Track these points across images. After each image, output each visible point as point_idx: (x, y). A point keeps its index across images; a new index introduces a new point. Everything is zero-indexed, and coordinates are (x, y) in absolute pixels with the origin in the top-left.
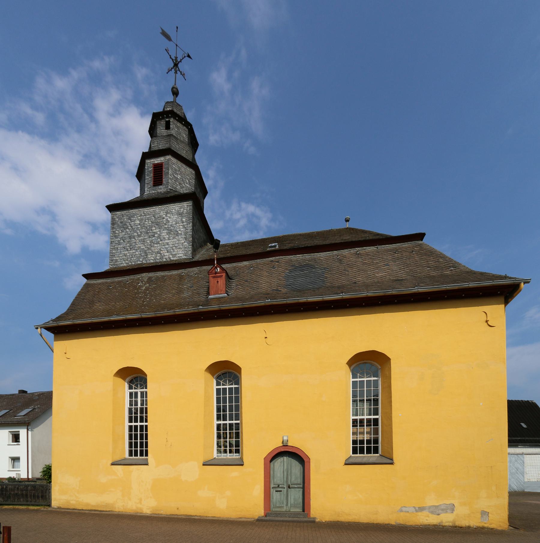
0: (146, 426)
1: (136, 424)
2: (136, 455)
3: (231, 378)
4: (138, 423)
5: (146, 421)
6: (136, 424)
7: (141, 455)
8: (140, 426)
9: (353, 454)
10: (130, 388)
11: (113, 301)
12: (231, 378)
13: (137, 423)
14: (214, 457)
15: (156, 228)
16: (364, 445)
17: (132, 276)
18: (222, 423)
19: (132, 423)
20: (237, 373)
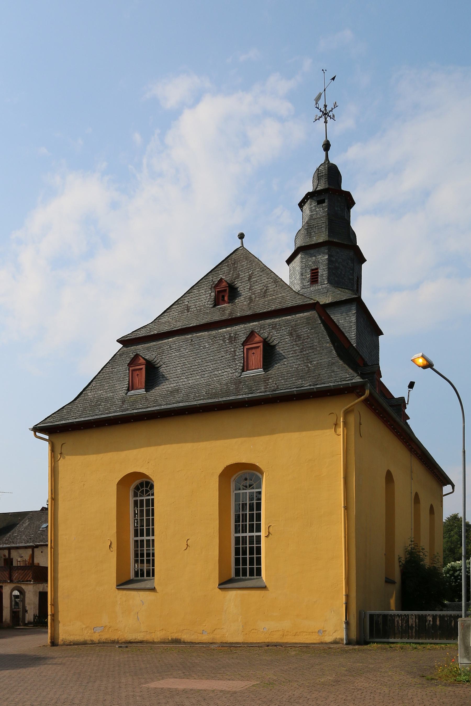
0: (153, 540)
1: (251, 534)
2: (245, 574)
3: (148, 488)
4: (144, 537)
5: (153, 535)
6: (251, 534)
7: (252, 574)
8: (249, 536)
9: (135, 577)
10: (135, 495)
11: (175, 362)
12: (148, 488)
13: (149, 537)
14: (132, 578)
15: (316, 210)
16: (249, 568)
17: (141, 336)
18: (255, 535)
19: (138, 537)
20: (252, 471)
